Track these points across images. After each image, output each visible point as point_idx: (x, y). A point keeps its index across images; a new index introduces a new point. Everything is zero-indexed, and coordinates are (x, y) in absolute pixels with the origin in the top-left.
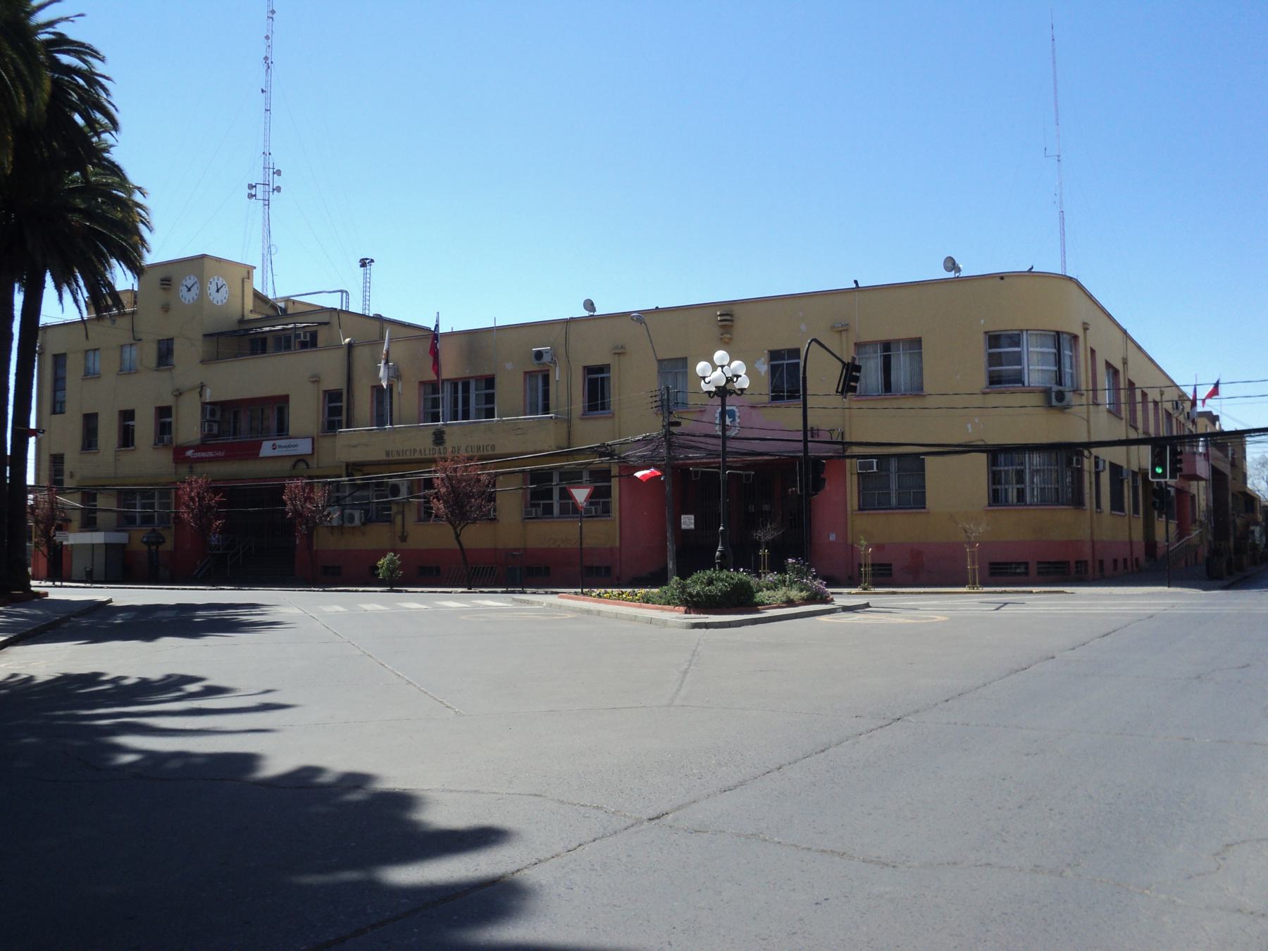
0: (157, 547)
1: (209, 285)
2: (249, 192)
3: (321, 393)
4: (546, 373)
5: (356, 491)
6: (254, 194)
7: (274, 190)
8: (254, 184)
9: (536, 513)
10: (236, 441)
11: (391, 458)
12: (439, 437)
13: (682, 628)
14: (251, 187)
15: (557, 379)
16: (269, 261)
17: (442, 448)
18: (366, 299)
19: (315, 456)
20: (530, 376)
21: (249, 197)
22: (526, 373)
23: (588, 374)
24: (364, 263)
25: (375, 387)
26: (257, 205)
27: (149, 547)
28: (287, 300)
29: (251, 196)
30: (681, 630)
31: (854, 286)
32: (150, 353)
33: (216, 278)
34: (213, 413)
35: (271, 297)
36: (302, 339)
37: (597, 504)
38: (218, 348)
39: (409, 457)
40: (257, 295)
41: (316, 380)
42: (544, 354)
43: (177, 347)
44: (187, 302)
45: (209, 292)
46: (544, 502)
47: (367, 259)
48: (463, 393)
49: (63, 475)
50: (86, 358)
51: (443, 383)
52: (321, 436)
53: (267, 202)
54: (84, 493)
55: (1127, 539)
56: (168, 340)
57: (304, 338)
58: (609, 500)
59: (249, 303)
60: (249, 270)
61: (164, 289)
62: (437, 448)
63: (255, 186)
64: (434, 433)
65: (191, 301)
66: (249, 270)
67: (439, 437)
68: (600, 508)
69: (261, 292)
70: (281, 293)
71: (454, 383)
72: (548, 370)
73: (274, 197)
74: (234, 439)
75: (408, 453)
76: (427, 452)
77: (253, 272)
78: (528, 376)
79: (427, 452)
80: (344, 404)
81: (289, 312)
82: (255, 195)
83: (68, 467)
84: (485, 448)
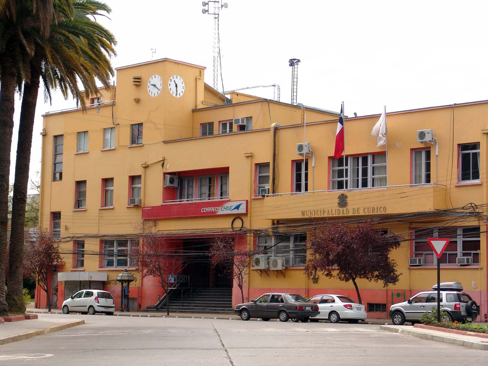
0: (128, 284)
1: (169, 82)
2: (204, 8)
3: (254, 166)
4: (428, 150)
5: (279, 243)
6: (207, 9)
7: (222, 6)
8: (207, 2)
9: (420, 262)
10: (188, 202)
11: (306, 217)
12: (343, 201)
13: (482, 349)
14: (205, 4)
15: (437, 154)
16: (219, 63)
17: (345, 209)
18: (294, 92)
19: (249, 215)
20: (416, 152)
21: (203, 13)
22: (412, 150)
23: (463, 150)
24: (293, 63)
25: (294, 161)
26: (209, 18)
27: (122, 284)
28: (232, 93)
29: (205, 11)
30: (480, 351)
31: (354, 116)
32: (126, 135)
33: (175, 76)
34: (172, 181)
35: (220, 90)
36: (240, 123)
37: (469, 254)
38: (193, 130)
39: (319, 216)
40: (208, 89)
41: (250, 156)
42: (426, 134)
43: (145, 130)
44: (153, 95)
45: (169, 87)
46: (128, 261)
47: (295, 59)
48: (363, 166)
49: (60, 227)
50: (79, 140)
51: (347, 159)
52: (253, 199)
53: (217, 17)
54: (102, 242)
55: (409, 289)
56: (139, 124)
57: (242, 123)
58: (478, 251)
59: (201, 95)
60: (201, 69)
61: (136, 85)
62: (341, 209)
63: (208, 4)
64: (339, 198)
65: (156, 95)
66: (201, 69)
67: (343, 201)
68: (471, 258)
69: (212, 87)
70: (229, 88)
71: (356, 157)
72: (430, 147)
73: (223, 12)
74: (188, 201)
75: (319, 213)
76: (334, 212)
77: (204, 72)
78: (414, 152)
79: (334, 212)
80: (271, 174)
81: (234, 102)
82: (208, 11)
83: (64, 221)
84: (378, 210)
